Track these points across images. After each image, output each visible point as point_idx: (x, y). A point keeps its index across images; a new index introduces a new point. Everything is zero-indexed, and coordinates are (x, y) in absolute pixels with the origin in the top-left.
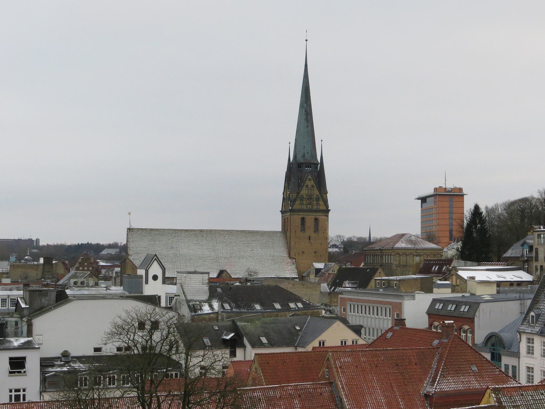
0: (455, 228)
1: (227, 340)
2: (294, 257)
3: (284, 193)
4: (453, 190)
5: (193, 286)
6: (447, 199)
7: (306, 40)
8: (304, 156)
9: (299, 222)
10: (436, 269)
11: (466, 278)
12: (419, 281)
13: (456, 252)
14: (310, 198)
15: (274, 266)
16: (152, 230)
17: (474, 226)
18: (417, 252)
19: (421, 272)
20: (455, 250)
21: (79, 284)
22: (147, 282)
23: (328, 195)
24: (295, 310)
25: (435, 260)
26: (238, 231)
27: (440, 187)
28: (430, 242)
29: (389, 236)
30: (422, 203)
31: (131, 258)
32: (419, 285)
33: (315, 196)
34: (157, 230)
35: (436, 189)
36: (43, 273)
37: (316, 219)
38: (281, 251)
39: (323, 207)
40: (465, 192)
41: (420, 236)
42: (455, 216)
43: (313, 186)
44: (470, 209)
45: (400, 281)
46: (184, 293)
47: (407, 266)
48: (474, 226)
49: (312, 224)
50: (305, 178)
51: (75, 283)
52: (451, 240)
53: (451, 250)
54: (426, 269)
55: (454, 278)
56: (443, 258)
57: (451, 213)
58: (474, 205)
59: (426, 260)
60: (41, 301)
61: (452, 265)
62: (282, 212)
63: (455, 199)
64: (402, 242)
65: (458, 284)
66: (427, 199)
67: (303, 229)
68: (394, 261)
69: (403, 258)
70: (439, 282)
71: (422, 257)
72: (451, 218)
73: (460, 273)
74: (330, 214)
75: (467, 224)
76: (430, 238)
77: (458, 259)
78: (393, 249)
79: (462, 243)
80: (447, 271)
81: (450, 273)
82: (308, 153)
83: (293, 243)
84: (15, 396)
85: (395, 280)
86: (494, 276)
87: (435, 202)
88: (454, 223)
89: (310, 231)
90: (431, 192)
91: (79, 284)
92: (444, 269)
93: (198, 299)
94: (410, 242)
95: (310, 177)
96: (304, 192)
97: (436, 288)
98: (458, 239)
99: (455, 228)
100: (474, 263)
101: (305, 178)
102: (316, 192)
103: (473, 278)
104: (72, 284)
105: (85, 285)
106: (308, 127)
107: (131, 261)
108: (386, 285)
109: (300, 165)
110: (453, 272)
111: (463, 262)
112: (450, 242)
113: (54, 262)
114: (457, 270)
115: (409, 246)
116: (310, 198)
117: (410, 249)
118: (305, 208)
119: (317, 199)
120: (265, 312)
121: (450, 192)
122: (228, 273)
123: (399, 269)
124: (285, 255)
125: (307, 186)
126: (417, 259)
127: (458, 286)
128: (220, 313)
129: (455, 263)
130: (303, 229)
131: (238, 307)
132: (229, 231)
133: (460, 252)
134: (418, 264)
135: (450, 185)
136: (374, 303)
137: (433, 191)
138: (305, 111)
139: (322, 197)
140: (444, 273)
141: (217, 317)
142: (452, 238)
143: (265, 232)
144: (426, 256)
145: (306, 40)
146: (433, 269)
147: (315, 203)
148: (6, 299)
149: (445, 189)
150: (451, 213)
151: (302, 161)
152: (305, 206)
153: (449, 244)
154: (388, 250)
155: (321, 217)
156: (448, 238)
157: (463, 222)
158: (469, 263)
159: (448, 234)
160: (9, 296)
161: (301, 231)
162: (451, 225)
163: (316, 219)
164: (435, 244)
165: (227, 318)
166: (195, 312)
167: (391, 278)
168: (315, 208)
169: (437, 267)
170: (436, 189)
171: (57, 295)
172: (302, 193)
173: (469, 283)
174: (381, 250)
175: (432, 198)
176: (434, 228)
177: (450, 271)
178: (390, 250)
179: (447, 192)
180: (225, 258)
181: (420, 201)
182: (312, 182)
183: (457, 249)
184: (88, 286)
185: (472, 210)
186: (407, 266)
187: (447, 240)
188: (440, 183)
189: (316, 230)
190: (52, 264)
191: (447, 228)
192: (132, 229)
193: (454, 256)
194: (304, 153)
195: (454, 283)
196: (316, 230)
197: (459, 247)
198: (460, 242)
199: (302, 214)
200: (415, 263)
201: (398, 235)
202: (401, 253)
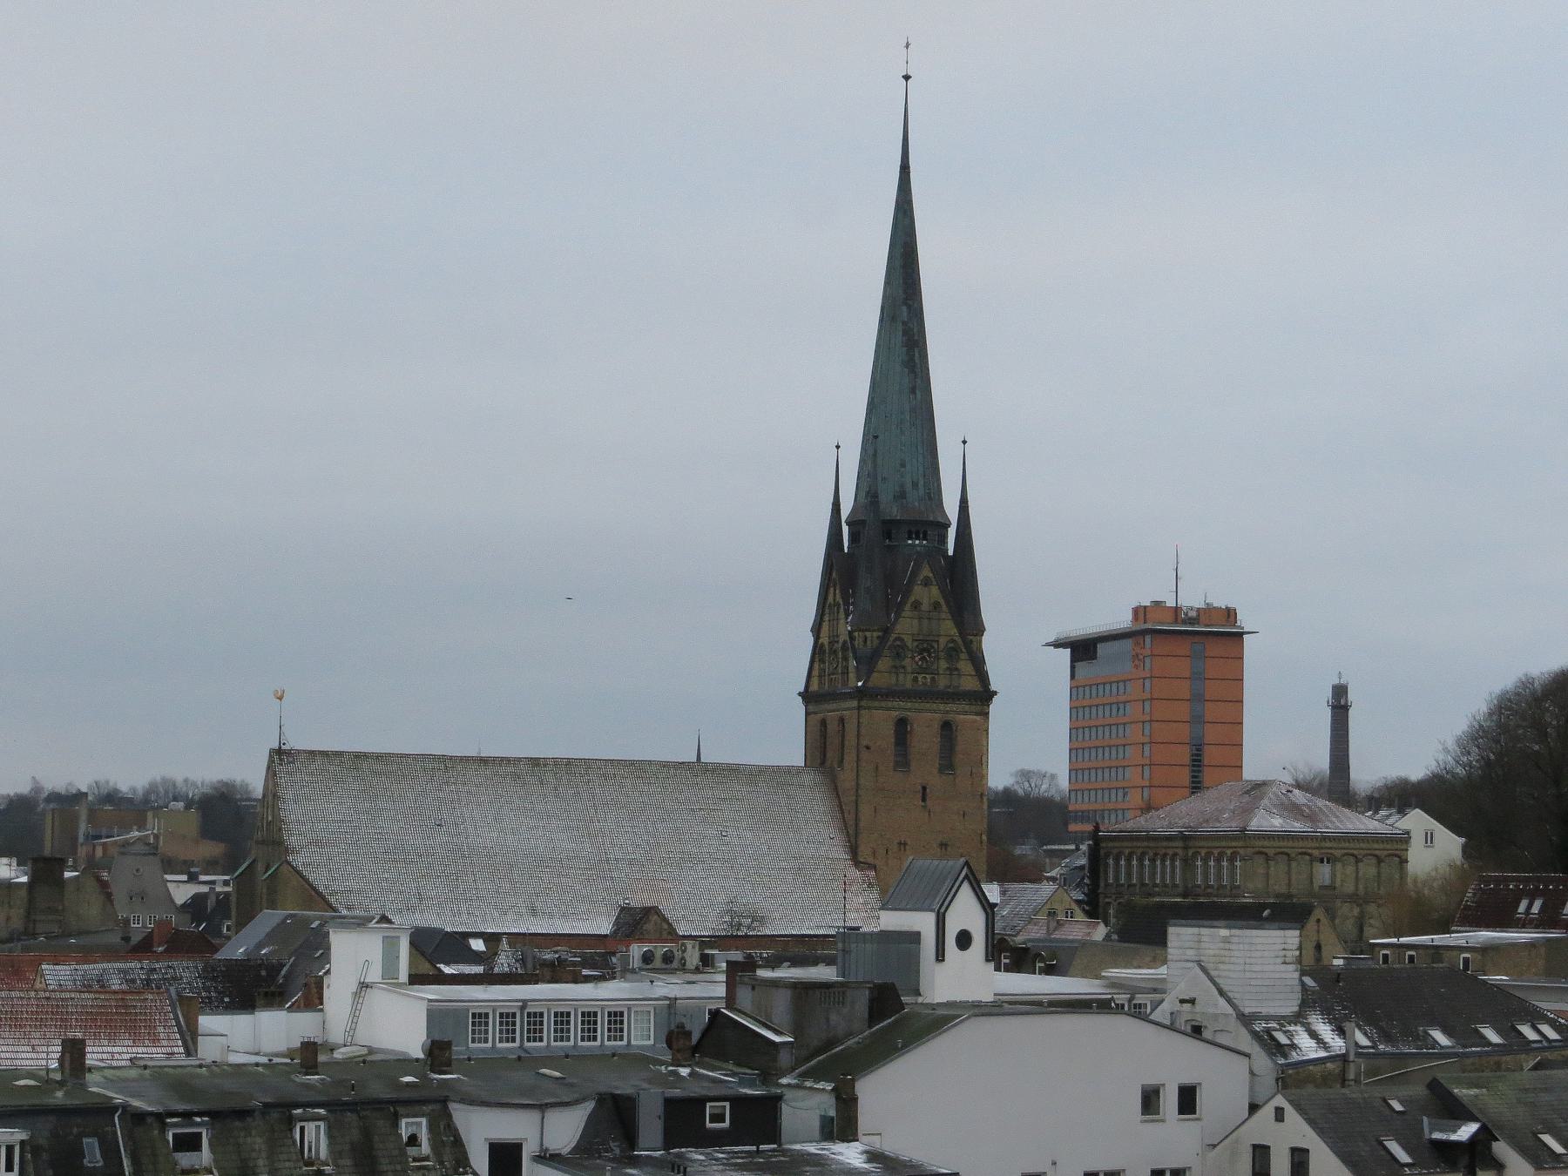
1: (1457, 1144)
2: (871, 860)
3: (816, 630)
4: (1208, 612)
5: (1257, 968)
7: (907, 78)
8: (901, 495)
9: (889, 731)
10: (1535, 909)
12: (1543, 951)
14: (926, 648)
15: (808, 890)
16: (359, 756)
21: (658, 963)
22: (940, 956)
23: (985, 639)
24: (1544, 1049)
26: (665, 765)
27: (1157, 604)
30: (1074, 660)
31: (298, 860)
33: (943, 641)
34: (379, 757)
36: (28, 913)
37: (947, 726)
38: (815, 833)
39: (969, 683)
40: (1245, 621)
43: (936, 606)
46: (1222, 993)
50: (897, 571)
51: (647, 958)
60: (828, 1020)
62: (806, 696)
74: (994, 708)
78: (1243, 835)
82: (915, 485)
83: (866, 811)
85: (1461, 949)
89: (925, 769)
90: (1122, 620)
91: (658, 963)
93: (1272, 1011)
95: (926, 572)
96: (907, 626)
101: (897, 571)
102: (948, 628)
104: (636, 962)
105: (675, 964)
106: (913, 391)
107: (299, 873)
109: (889, 528)
113: (67, 874)
115: (1297, 826)
116: (926, 648)
117: (1303, 838)
118: (909, 685)
119: (952, 653)
120: (1466, 1055)
121: (1192, 621)
122: (665, 920)
124: (840, 853)
125: (916, 606)
128: (1352, 1058)
131: (1387, 1037)
132: (632, 763)
135: (1192, 599)
137: (1129, 616)
138: (905, 333)
139: (968, 644)
141: (1344, 1071)
143: (762, 771)
144: (1374, 861)
145: (907, 78)
146: (1522, 909)
147: (943, 664)
148: (514, 1015)
149: (1177, 610)
151: (894, 512)
152: (910, 677)
154: (1225, 838)
155: (963, 717)
160: (525, 1003)
161: (897, 764)
163: (947, 726)
165: (1368, 1076)
166: (1285, 1056)
168: (942, 682)
171: (872, 1001)
172: (899, 628)
174: (1183, 837)
175: (1127, 644)
178: (1235, 838)
179: (1184, 622)
180: (631, 863)
182: (935, 590)
184: (683, 968)
188: (1157, 590)
189: (947, 763)
190: (61, 882)
192: (289, 753)
194: (902, 486)
196: (947, 763)
199: (898, 709)
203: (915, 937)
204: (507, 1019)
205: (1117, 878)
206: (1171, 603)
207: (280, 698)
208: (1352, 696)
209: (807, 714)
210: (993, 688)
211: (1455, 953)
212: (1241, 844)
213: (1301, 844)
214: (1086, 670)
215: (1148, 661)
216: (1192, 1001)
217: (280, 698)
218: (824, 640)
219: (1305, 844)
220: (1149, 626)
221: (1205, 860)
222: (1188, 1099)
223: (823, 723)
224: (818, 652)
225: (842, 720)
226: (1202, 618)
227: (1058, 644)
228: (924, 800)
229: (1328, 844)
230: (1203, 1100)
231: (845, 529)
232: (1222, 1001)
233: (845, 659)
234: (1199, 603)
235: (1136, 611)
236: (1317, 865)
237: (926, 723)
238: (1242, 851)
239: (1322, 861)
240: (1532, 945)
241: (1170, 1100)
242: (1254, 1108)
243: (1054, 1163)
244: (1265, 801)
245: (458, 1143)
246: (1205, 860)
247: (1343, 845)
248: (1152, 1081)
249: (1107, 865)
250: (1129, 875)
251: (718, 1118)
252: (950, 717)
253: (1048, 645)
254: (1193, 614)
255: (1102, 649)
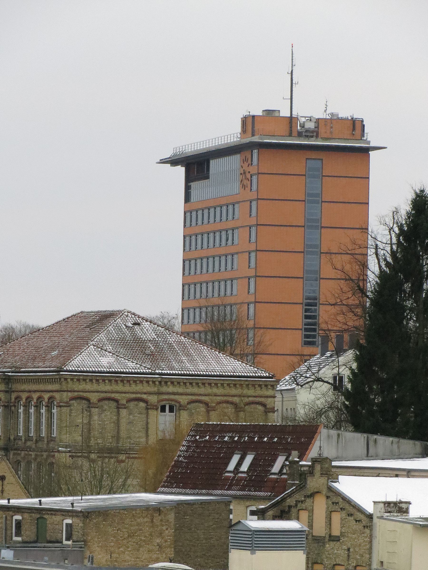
0: (328, 290)
4: (334, 122)
6: (296, 164)
10: (245, 467)
11: (370, 508)
12: (171, 517)
13: (331, 396)
17: (407, 286)
18: (167, 393)
19: (179, 479)
20: (325, 387)
25: (241, 430)
27: (269, 113)
28: (221, 348)
29: (44, 318)
30: (189, 179)
32: (169, 533)
35: (249, 123)
40: (372, 136)
41: (178, 327)
42: (330, 240)
44: (396, 212)
45: (86, 515)
47: (119, 451)
48: (407, 286)
52: (309, 341)
53: (309, 390)
54: (198, 465)
55: (320, 505)
56: (275, 419)
57: (313, 224)
58: (411, 196)
59: (199, 429)
61: (313, 453)
63: (333, 165)
64: (100, 348)
65: (336, 532)
66: (213, 163)
68: (65, 428)
69: (103, 419)
70: (255, 524)
71: (184, 415)
72: (311, 249)
73: (347, 485)
75: (382, 275)
76: (220, 333)
77: (337, 425)
78: (58, 375)
79: (357, 359)
80: (291, 475)
81: (301, 487)
86: (113, 502)
87: (245, 179)
88: (327, 271)
90: (229, 132)
92: (276, 468)
94: (134, 345)
97: (241, 547)
98: (340, 338)
99: (328, 290)
100: (407, 445)
103: (399, 508)
108: (29, 532)
110: (315, 482)
111: (356, 440)
112: (308, 350)
114: (331, 474)
115: (131, 366)
121: (313, 133)
123: (86, 464)
126: (164, 422)
127: (336, 539)
129: (323, 444)
133: (348, 395)
134: (165, 446)
135: (309, 108)
137: (239, 129)
140: (278, 486)
142: (312, 334)
144: (202, 409)
146: (231, 466)
150: (313, 224)
153: (304, 358)
156: (299, 336)
157: (364, 266)
158: (384, 442)
159: (297, 317)
162: (313, 276)
164: (241, 357)
167: (48, 502)
169: (249, 459)
173: (383, 528)
175: (235, 160)
176: (238, 292)
177: (303, 476)
179: (300, 135)
181: (181, 170)
183: (337, 384)
185: (402, 217)
186: (119, 451)
187: (294, 341)
191: (296, 291)
193: (320, 413)
195: (320, 529)
197: (346, 373)
198: (349, 356)
200: (152, 440)
201: (81, 316)
202: (94, 398)
205: (27, 429)
206: (285, 113)
211: (58, 518)
212: (56, 387)
213: (134, 388)
215: (255, 178)
219: (139, 388)
220: (256, 139)
221: (27, 406)
226: (322, 130)
229: (171, 389)
235: (244, 121)
236: (152, 413)
238: (57, 395)
239: (163, 409)
240: (158, 509)
244: (102, 336)
246: (27, 406)
247: (190, 390)
253: (163, 162)
254: (311, 125)
255: (215, 165)
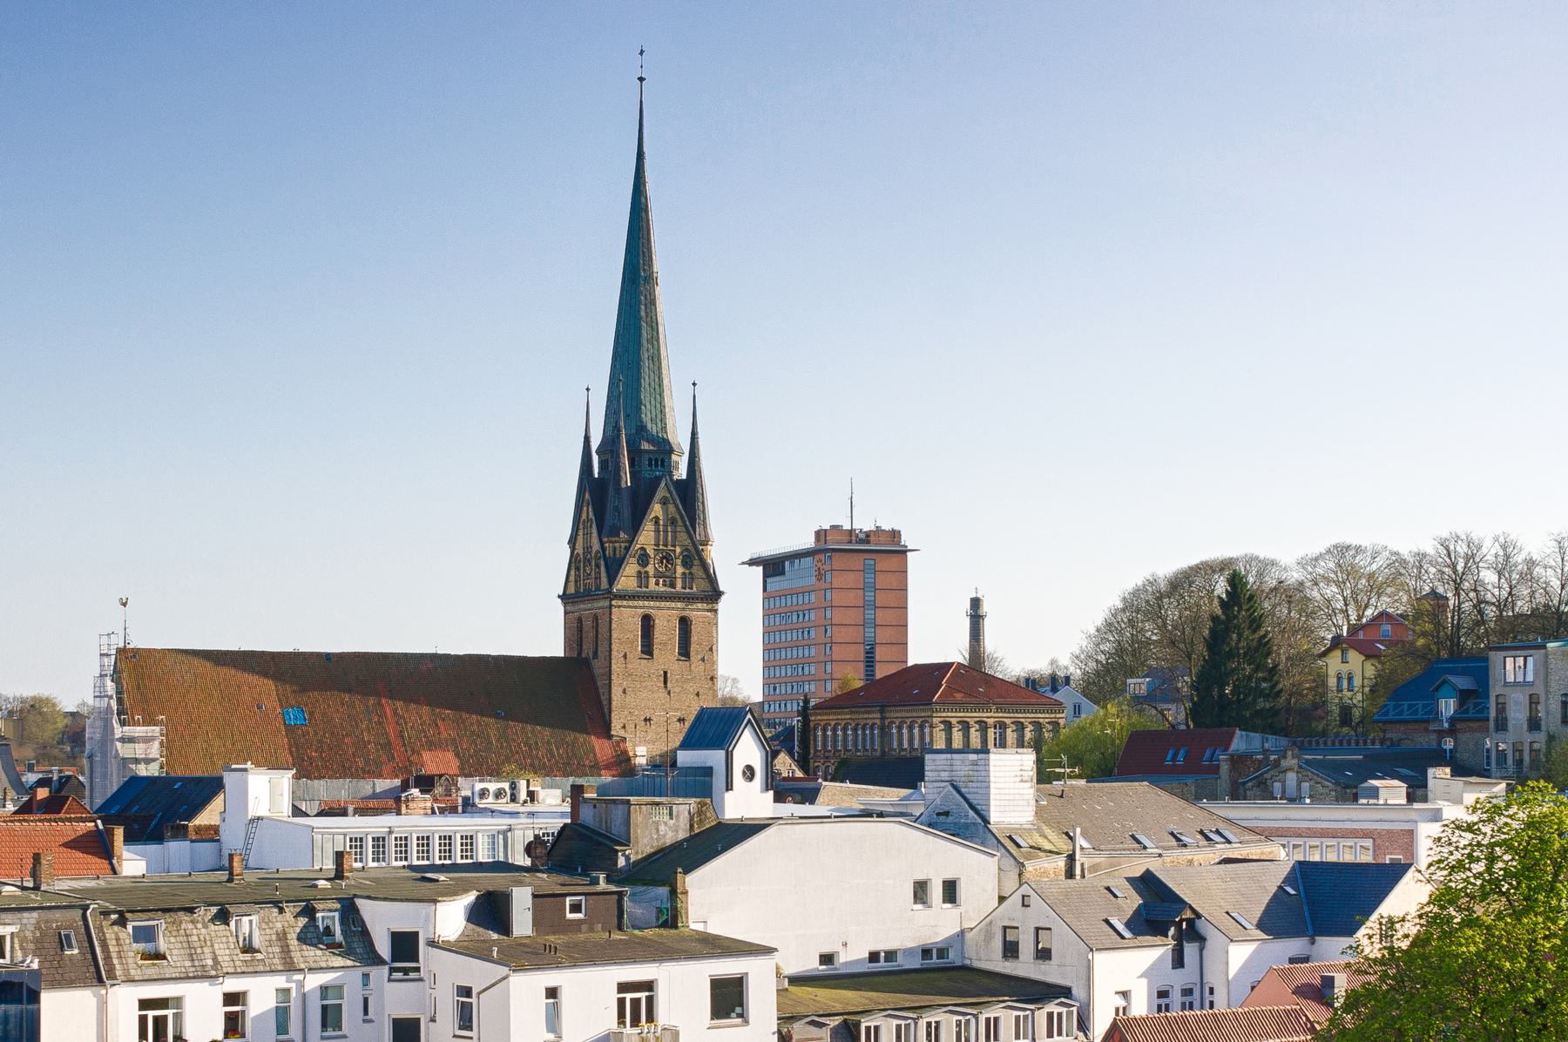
3: (572, 542)
6: (856, 562)
7: (641, 79)
22: (729, 786)
30: (766, 576)
35: (820, 534)
40: (907, 540)
49: (659, 636)
62: (565, 597)
67: (648, 649)
74: (722, 605)
84: (156, 1019)
89: (667, 653)
90: (808, 542)
130: (648, 649)
135: (864, 524)
136: (1300, 836)
149: (851, 532)
163: (685, 623)
170: (820, 534)
189: (685, 652)
199: (649, 606)
203: (708, 771)
204: (379, 842)
206: (847, 527)
207: (125, 605)
208: (986, 608)
209: (566, 613)
210: (721, 589)
214: (776, 583)
216: (947, 814)
217: (125, 605)
218: (579, 549)
222: (950, 891)
223: (580, 620)
224: (574, 562)
225: (596, 618)
226: (872, 538)
227: (753, 562)
228: (665, 682)
230: (963, 891)
231: (595, 458)
232: (971, 813)
233: (598, 566)
234: (868, 526)
235: (818, 533)
237: (666, 619)
241: (936, 892)
242: (1002, 899)
243: (845, 944)
245: (365, 934)
248: (921, 877)
249: (815, 736)
250: (835, 741)
251: (576, 908)
252: (685, 613)
254: (862, 536)
